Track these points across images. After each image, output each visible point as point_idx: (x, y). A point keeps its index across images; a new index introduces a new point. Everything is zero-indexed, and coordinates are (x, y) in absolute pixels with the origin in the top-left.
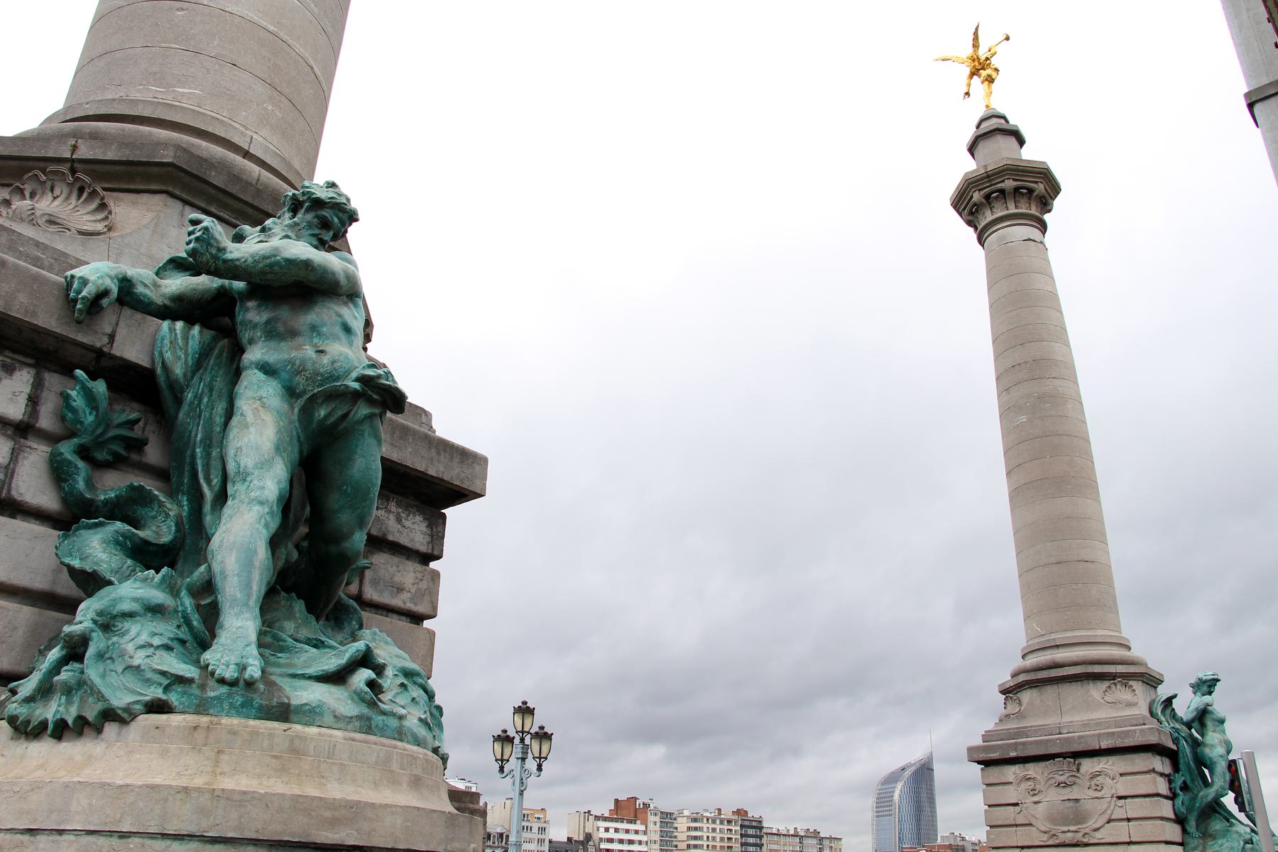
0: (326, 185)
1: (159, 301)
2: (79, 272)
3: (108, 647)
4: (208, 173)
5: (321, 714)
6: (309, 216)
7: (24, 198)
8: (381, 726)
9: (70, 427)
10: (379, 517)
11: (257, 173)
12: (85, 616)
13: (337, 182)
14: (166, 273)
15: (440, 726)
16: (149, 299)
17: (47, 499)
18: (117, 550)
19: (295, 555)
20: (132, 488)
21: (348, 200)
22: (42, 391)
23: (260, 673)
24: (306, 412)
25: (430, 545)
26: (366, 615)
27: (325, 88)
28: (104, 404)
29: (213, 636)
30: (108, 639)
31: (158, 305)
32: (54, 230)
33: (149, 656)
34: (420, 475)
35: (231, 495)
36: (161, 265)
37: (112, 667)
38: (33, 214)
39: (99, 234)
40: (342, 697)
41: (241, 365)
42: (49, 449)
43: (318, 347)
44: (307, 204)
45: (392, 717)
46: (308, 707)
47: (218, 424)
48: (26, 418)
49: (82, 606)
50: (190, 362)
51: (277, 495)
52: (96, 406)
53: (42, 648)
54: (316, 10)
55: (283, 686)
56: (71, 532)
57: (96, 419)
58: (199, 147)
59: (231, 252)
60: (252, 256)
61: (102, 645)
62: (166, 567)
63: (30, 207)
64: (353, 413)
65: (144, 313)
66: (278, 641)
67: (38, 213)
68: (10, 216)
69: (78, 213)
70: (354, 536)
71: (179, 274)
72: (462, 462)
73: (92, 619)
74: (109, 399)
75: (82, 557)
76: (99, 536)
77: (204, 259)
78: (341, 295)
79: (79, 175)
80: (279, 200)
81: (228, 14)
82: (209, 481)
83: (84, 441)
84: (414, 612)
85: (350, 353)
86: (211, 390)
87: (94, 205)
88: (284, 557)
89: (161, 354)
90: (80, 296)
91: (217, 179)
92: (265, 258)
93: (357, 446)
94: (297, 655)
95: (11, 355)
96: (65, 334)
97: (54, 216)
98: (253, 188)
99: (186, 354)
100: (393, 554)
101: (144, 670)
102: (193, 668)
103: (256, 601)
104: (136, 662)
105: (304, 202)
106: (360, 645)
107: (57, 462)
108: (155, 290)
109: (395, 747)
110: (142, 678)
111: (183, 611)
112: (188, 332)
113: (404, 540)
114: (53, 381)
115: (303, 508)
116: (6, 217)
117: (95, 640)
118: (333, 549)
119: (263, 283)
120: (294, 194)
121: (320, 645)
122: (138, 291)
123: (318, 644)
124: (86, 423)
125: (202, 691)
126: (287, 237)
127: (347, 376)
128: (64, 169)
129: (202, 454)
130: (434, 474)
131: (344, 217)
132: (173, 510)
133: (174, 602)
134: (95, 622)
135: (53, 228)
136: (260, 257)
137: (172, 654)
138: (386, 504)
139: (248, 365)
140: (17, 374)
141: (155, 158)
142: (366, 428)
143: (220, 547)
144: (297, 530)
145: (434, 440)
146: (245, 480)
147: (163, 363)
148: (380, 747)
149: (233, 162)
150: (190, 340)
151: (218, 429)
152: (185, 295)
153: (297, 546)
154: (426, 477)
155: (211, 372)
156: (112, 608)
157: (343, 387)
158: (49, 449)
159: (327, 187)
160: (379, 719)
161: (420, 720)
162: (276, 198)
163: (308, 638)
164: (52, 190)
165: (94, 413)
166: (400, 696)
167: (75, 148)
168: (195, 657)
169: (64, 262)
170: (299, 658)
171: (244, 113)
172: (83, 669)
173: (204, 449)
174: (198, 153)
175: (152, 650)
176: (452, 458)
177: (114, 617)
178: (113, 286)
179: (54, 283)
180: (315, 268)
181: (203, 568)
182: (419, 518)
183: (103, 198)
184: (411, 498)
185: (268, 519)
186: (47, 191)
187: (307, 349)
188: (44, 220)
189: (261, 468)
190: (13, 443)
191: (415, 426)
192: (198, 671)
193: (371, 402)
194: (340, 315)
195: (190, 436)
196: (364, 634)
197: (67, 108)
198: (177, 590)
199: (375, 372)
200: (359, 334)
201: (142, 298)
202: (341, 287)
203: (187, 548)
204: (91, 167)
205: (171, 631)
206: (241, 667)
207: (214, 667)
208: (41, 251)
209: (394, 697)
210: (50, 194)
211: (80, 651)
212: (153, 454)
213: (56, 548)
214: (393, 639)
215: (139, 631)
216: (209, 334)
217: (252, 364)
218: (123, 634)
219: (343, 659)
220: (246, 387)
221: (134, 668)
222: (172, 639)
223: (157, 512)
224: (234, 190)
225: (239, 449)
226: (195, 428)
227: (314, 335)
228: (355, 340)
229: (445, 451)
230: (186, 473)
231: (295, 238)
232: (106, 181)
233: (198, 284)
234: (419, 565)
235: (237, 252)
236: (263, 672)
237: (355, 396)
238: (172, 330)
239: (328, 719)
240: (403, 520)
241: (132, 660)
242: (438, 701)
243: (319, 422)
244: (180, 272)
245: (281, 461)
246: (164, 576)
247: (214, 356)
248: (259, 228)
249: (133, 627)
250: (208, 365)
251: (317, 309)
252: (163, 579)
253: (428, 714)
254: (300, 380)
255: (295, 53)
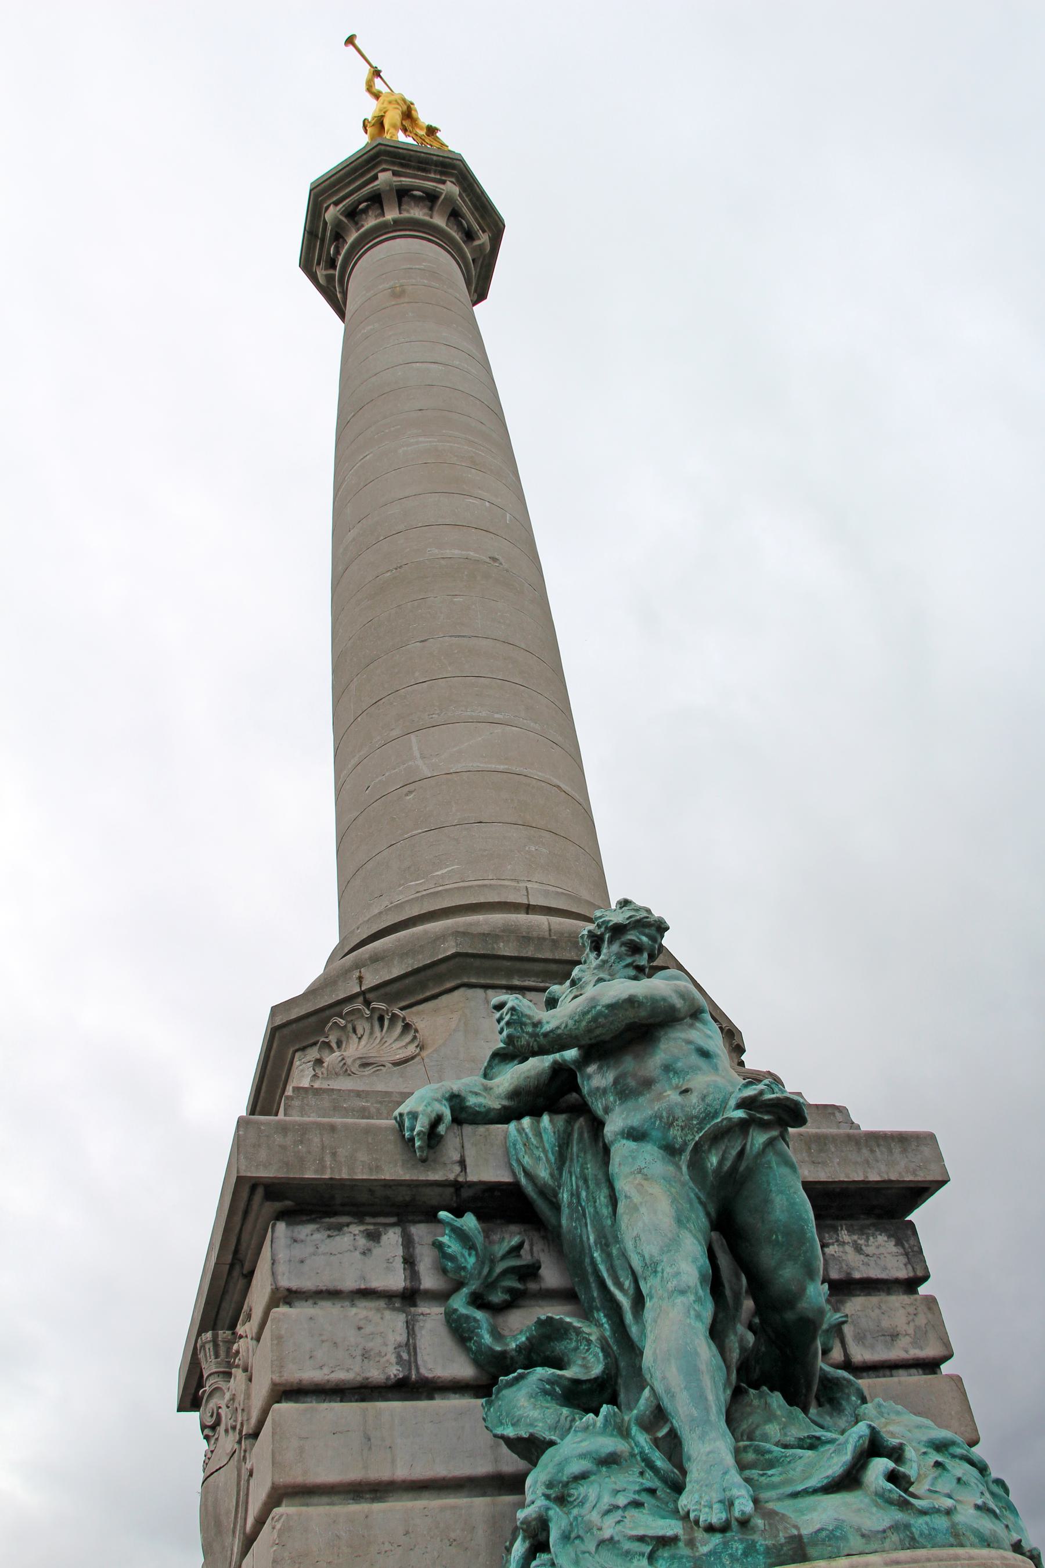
0: (619, 906)
1: (496, 1105)
2: (404, 1108)
3: (571, 1524)
4: (495, 946)
5: (844, 1538)
6: (615, 947)
7: (332, 1051)
8: (926, 1532)
9: (454, 1277)
10: (833, 1255)
11: (546, 923)
12: (536, 1493)
13: (629, 898)
14: (494, 1070)
15: (1010, 1507)
16: (485, 1106)
17: (463, 1369)
18: (547, 1402)
19: (750, 1338)
20: (540, 1323)
21: (648, 911)
22: (414, 1248)
23: (751, 1504)
24: (696, 1165)
25: (909, 1267)
26: (864, 1383)
27: (581, 801)
28: (479, 1240)
29: (684, 1473)
30: (568, 1513)
31: (497, 1110)
32: (369, 1072)
33: (619, 1522)
34: (862, 1186)
35: (647, 1295)
36: (486, 1064)
37: (583, 1548)
38: (345, 1064)
39: (413, 1058)
40: (862, 1506)
41: (606, 1141)
42: (442, 1310)
43: (681, 1087)
44: (607, 936)
45: (936, 1515)
46: (824, 1533)
47: (607, 1217)
48: (408, 1284)
49: (529, 1481)
50: (552, 1159)
51: (698, 1276)
52: (473, 1245)
53: (508, 1544)
54: (537, 727)
55: (786, 1512)
56: (494, 1396)
57: (477, 1260)
58: (477, 924)
59: (548, 1023)
60: (571, 1017)
61: (564, 1523)
62: (605, 1406)
63: (340, 1058)
64: (748, 1147)
65: (486, 1124)
66: (763, 1455)
67: (349, 1061)
68: (325, 1075)
69: (387, 1044)
70: (808, 1291)
71: (508, 1066)
72: (904, 1151)
73: (544, 1495)
74: (484, 1231)
75: (513, 1422)
76: (523, 1392)
77: (523, 1042)
78: (682, 1019)
79: (374, 1005)
80: (578, 942)
81: (454, 775)
82: (620, 1285)
83: (474, 1287)
84: (924, 1359)
85: (719, 1079)
86: (586, 1181)
87: (399, 1029)
88: (737, 1345)
89: (518, 1161)
90: (415, 1133)
91: (506, 949)
92: (585, 1014)
93: (768, 1183)
94: (792, 1465)
95: (372, 1220)
96: (415, 1178)
97: (365, 1058)
98: (548, 941)
99: (545, 1151)
100: (869, 1294)
101: (619, 1541)
102: (673, 1522)
103: (717, 1413)
104: (607, 1534)
105: (602, 935)
106: (861, 1429)
107: (455, 1321)
108: (489, 1093)
109: (956, 1558)
110: (620, 1551)
111: (641, 1453)
112: (538, 1126)
113: (875, 1273)
114: (420, 1231)
115: (739, 1279)
116: (322, 1078)
117: (555, 1519)
118: (790, 1316)
119: (593, 1041)
120: (589, 931)
121: (817, 1442)
122: (471, 1103)
123: (813, 1444)
124: (469, 1267)
125: (692, 1549)
126: (600, 980)
127: (725, 1107)
128: (358, 1005)
129: (601, 1257)
130: (878, 1178)
131: (650, 931)
132: (592, 1332)
133: (626, 1445)
134: (547, 1497)
135: (368, 1071)
136: (579, 1015)
137: (644, 1511)
138: (835, 1236)
139: (614, 1138)
140: (384, 1238)
141: (438, 956)
142: (771, 1157)
143: (655, 1361)
144: (741, 1308)
145: (862, 1135)
146: (656, 1272)
147: (525, 1171)
148: (936, 1563)
149: (518, 924)
150: (543, 1135)
151: (609, 1222)
152: (520, 1088)
153: (751, 1327)
154: (869, 1186)
155: (578, 1161)
156: (560, 1474)
157: (725, 1122)
158: (442, 1310)
159: (621, 908)
160: (919, 1523)
161: (977, 1507)
162: (573, 939)
163: (800, 1439)
164: (354, 1031)
165: (474, 1253)
166: (940, 1480)
167: (360, 979)
168: (671, 1506)
169: (389, 1102)
170: (794, 1470)
171: (509, 867)
172: (552, 1559)
173: (602, 1250)
174: (480, 930)
175: (620, 1512)
176: (890, 1151)
177: (566, 1485)
178: (444, 1108)
179: (386, 1129)
180: (642, 1002)
181: (647, 1392)
182: (882, 1238)
183: (404, 1019)
184: (862, 1216)
185: (697, 1308)
186: (350, 1034)
187: (669, 1095)
188: (357, 1066)
189: (669, 1251)
190: (404, 1315)
191: (832, 1130)
192: (679, 1524)
193: (764, 1125)
194: (689, 1042)
195: (581, 1241)
196: (866, 1411)
197: (343, 940)
198: (627, 1429)
199: (755, 1089)
200: (720, 1052)
201: (477, 1109)
202: (679, 1010)
203: (624, 1373)
204: (382, 991)
205: (635, 1482)
206: (727, 1503)
207: (696, 1513)
208: (364, 1100)
209: (933, 1484)
210: (354, 1036)
211: (541, 1537)
212: (551, 1276)
213: (484, 1420)
214: (905, 1407)
215: (599, 1494)
216: (561, 1119)
217: (618, 1134)
218: (582, 1503)
219: (846, 1453)
220: (620, 1164)
221: (607, 1542)
222: (638, 1492)
223: (577, 1341)
224: (529, 952)
225: (637, 1238)
226: (584, 1230)
227: (671, 1076)
228: (719, 1062)
229: (878, 1146)
230: (593, 1285)
231: (609, 977)
232: (401, 999)
233: (529, 1070)
234: (905, 1297)
235: (552, 1020)
236: (756, 1501)
237: (744, 1126)
238: (521, 1131)
239: (856, 1542)
240: (864, 1248)
241: (601, 1532)
242: (994, 1473)
243: (714, 1171)
244: (507, 1064)
245: (688, 1235)
246: (606, 1417)
247: (575, 1142)
248: (568, 983)
249: (590, 1490)
250: (572, 1154)
251: (663, 1045)
252: (606, 1419)
253: (987, 1495)
254: (674, 1132)
255: (534, 781)
